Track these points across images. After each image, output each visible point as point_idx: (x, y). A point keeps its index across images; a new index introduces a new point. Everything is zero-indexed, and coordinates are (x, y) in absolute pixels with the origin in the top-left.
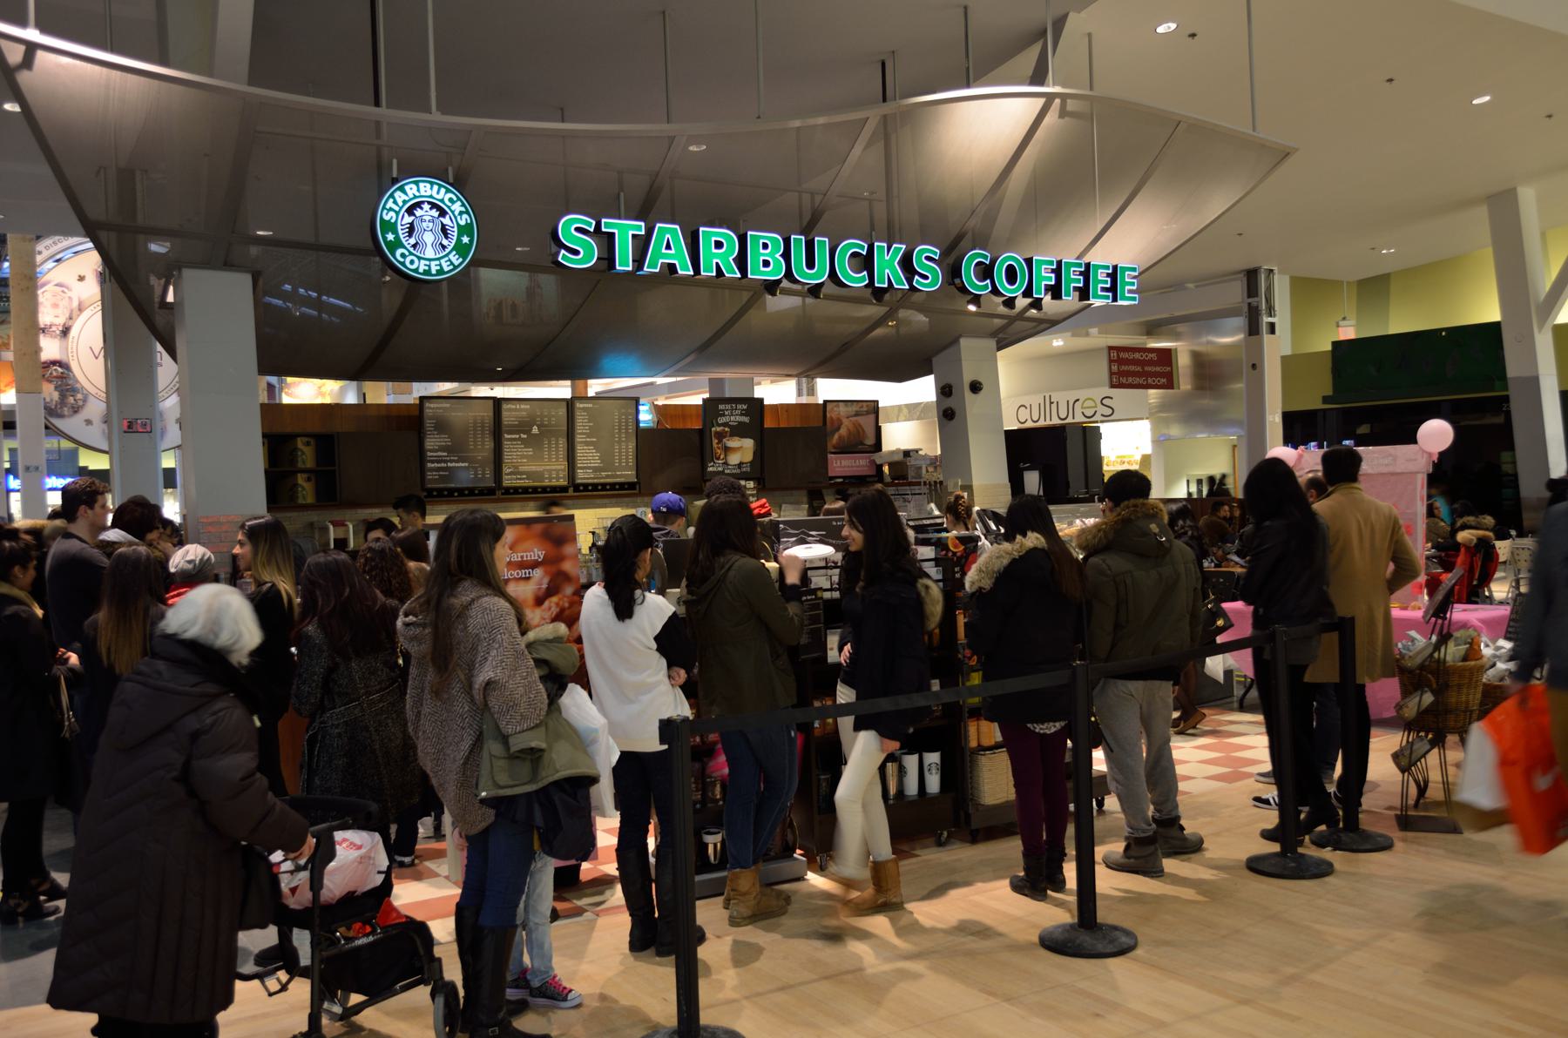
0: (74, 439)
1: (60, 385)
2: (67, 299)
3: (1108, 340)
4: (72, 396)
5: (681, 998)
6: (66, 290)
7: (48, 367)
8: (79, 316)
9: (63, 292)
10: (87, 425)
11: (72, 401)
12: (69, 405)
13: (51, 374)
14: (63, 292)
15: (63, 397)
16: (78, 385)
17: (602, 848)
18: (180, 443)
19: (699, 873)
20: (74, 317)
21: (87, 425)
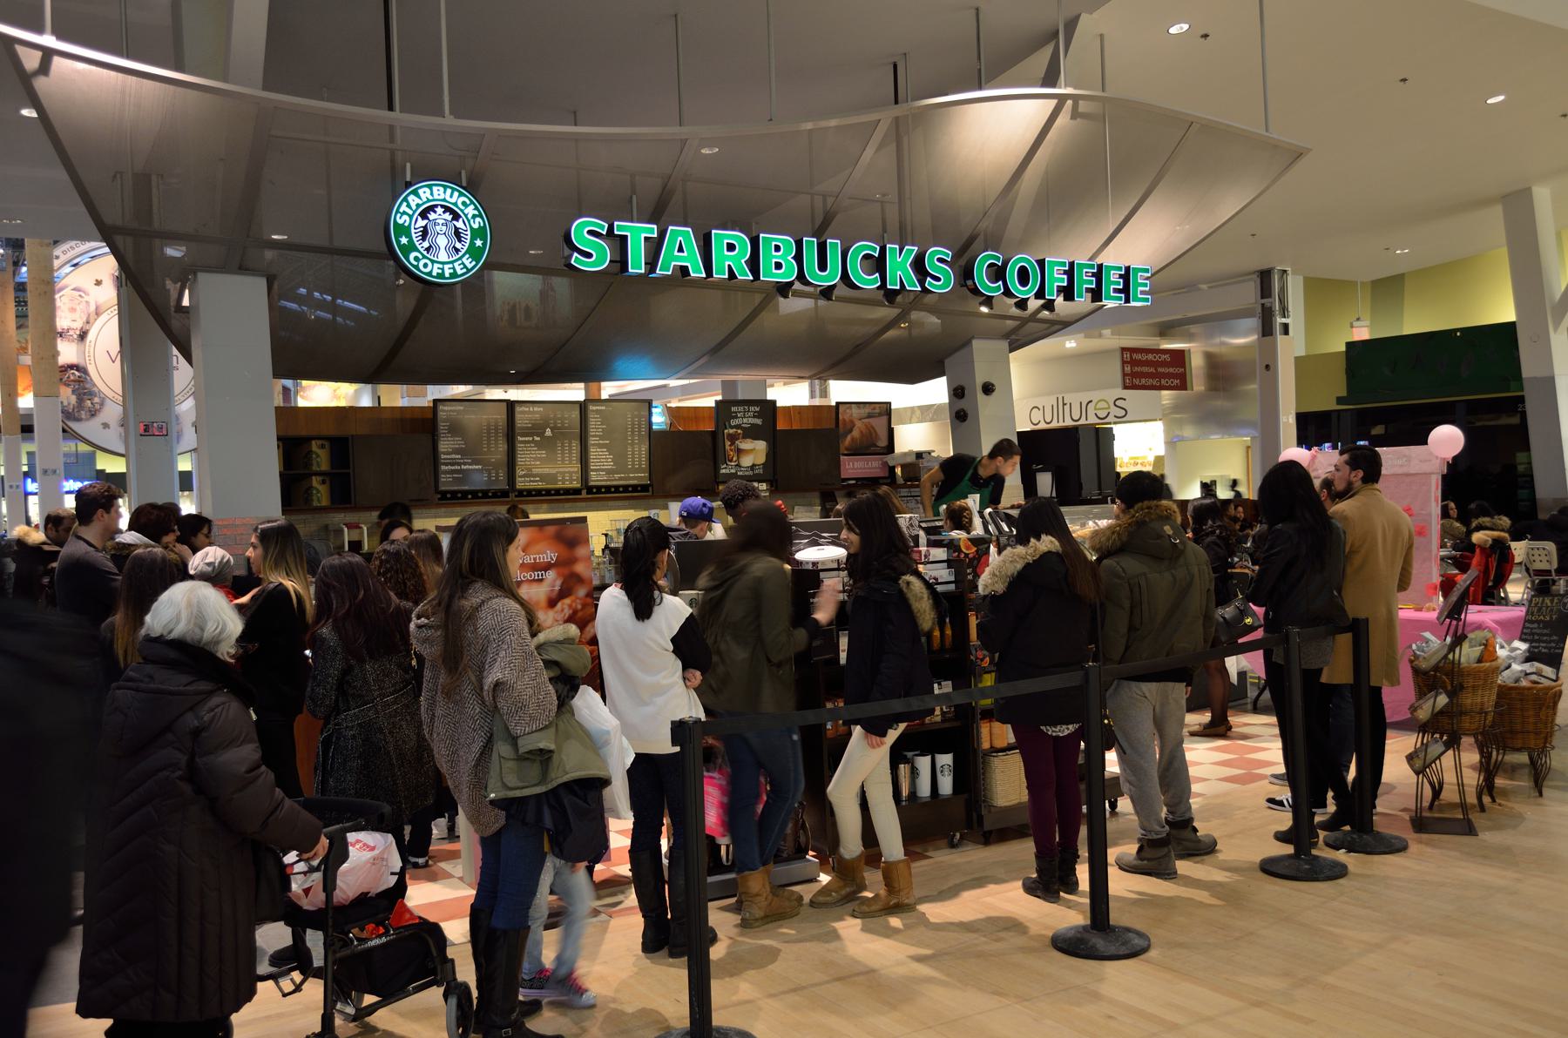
6: (83, 295)
11: (90, 405)
13: (69, 377)
15: (80, 400)
16: (95, 389)
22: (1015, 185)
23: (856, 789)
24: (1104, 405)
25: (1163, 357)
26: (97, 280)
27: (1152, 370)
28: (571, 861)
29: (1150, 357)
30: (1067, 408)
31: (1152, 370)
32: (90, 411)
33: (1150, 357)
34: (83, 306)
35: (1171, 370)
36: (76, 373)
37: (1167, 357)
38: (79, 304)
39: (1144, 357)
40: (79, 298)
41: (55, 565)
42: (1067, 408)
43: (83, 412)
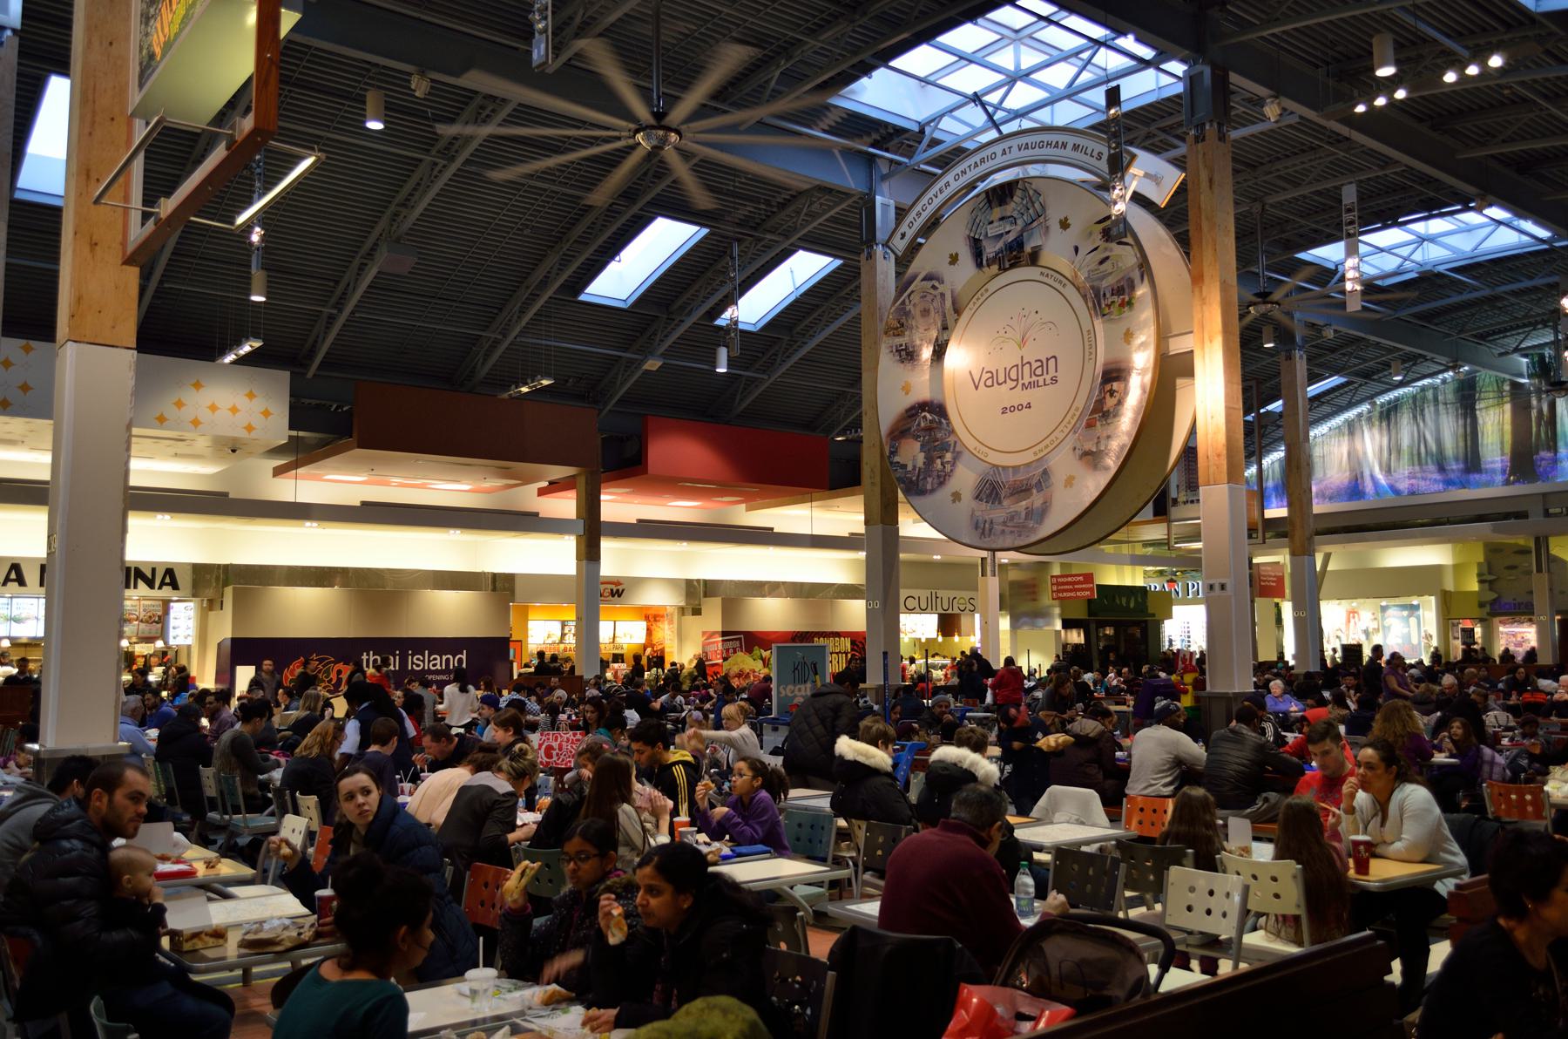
0: (993, 70)
1: (928, 442)
2: (939, 297)
3: (1413, 24)
4: (940, 457)
5: (737, 276)
6: (937, 284)
7: (916, 415)
8: (956, 321)
9: (934, 287)
10: (951, 256)
11: (939, 467)
12: (935, 474)
13: (919, 424)
14: (934, 287)
15: (929, 461)
16: (951, 439)
17: (36, 157)
18: (144, 122)
19: (1309, 385)
20: (950, 325)
21: (951, 256)
22: (1196, 461)
23: (1388, 824)
24: (963, 602)
25: (1078, 578)
26: (1066, 219)
27: (1071, 587)
28: (122, 603)
29: (1069, 579)
30: (939, 600)
31: (1071, 587)
32: (939, 477)
33: (1069, 579)
34: (937, 303)
35: (1084, 586)
36: (928, 415)
37: (1081, 578)
38: (932, 300)
39: (1065, 580)
40: (932, 291)
41: (1163, 675)
42: (939, 600)
43: (929, 480)
